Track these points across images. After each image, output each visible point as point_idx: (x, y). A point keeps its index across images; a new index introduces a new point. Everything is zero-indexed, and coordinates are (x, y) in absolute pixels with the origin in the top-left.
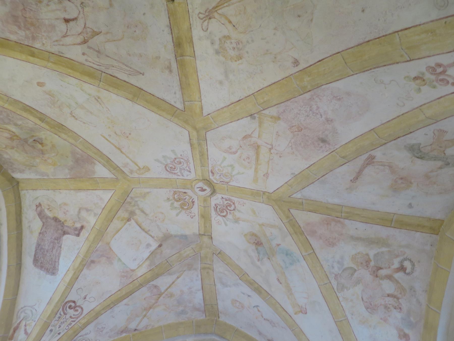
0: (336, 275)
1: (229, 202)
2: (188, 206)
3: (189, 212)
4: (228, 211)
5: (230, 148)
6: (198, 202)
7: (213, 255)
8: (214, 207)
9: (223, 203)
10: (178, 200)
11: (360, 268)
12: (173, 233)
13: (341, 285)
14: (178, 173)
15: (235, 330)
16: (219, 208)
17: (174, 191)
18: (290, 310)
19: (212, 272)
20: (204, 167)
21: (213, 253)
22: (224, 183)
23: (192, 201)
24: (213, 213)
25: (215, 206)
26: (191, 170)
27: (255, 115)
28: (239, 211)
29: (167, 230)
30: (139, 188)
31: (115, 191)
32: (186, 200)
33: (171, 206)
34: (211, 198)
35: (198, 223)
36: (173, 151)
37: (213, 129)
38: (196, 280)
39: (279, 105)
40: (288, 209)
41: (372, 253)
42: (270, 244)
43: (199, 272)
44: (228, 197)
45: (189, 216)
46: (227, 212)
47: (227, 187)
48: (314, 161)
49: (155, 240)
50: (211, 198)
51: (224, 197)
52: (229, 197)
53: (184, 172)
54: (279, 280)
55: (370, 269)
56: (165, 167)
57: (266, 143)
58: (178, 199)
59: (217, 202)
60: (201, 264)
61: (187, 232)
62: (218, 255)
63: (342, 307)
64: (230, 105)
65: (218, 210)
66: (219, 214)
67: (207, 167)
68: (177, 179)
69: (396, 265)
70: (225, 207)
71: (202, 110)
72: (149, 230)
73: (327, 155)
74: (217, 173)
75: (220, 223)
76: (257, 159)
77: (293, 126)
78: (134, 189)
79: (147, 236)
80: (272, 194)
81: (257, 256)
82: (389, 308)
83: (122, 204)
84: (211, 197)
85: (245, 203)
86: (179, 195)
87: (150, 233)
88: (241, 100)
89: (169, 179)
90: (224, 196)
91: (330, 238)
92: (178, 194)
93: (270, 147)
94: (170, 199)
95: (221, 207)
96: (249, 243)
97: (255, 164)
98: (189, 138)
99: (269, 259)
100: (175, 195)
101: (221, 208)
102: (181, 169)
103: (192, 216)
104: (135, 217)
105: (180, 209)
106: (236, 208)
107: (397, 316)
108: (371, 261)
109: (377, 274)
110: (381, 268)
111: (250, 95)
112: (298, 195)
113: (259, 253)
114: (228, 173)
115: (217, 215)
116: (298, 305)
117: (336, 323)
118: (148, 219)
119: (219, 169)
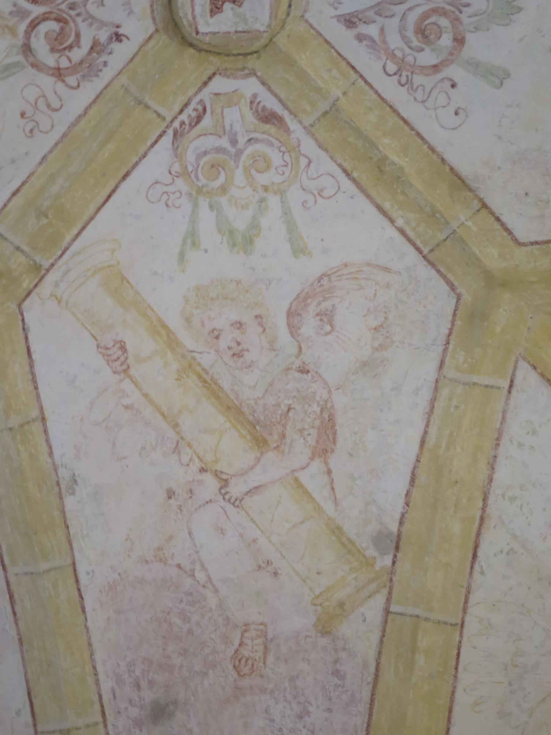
1: (77, 55)
9: (91, 17)
20: (326, 113)
22: (184, 117)
26: (350, 34)
27: (388, 560)
39: (370, 679)
44: (105, 70)
47: (159, 115)
51: (115, 46)
52: (107, 74)
57: (256, 488)
67: (312, 126)
70: (63, 7)
71: (542, 375)
73: (97, 682)
74: (257, 140)
77: (266, 650)
80: (14, 307)
85: (31, 131)
88: (472, 568)
97: (194, 359)
98: (494, 209)
106: (30, 69)
111: (465, 611)
119: (268, 167)
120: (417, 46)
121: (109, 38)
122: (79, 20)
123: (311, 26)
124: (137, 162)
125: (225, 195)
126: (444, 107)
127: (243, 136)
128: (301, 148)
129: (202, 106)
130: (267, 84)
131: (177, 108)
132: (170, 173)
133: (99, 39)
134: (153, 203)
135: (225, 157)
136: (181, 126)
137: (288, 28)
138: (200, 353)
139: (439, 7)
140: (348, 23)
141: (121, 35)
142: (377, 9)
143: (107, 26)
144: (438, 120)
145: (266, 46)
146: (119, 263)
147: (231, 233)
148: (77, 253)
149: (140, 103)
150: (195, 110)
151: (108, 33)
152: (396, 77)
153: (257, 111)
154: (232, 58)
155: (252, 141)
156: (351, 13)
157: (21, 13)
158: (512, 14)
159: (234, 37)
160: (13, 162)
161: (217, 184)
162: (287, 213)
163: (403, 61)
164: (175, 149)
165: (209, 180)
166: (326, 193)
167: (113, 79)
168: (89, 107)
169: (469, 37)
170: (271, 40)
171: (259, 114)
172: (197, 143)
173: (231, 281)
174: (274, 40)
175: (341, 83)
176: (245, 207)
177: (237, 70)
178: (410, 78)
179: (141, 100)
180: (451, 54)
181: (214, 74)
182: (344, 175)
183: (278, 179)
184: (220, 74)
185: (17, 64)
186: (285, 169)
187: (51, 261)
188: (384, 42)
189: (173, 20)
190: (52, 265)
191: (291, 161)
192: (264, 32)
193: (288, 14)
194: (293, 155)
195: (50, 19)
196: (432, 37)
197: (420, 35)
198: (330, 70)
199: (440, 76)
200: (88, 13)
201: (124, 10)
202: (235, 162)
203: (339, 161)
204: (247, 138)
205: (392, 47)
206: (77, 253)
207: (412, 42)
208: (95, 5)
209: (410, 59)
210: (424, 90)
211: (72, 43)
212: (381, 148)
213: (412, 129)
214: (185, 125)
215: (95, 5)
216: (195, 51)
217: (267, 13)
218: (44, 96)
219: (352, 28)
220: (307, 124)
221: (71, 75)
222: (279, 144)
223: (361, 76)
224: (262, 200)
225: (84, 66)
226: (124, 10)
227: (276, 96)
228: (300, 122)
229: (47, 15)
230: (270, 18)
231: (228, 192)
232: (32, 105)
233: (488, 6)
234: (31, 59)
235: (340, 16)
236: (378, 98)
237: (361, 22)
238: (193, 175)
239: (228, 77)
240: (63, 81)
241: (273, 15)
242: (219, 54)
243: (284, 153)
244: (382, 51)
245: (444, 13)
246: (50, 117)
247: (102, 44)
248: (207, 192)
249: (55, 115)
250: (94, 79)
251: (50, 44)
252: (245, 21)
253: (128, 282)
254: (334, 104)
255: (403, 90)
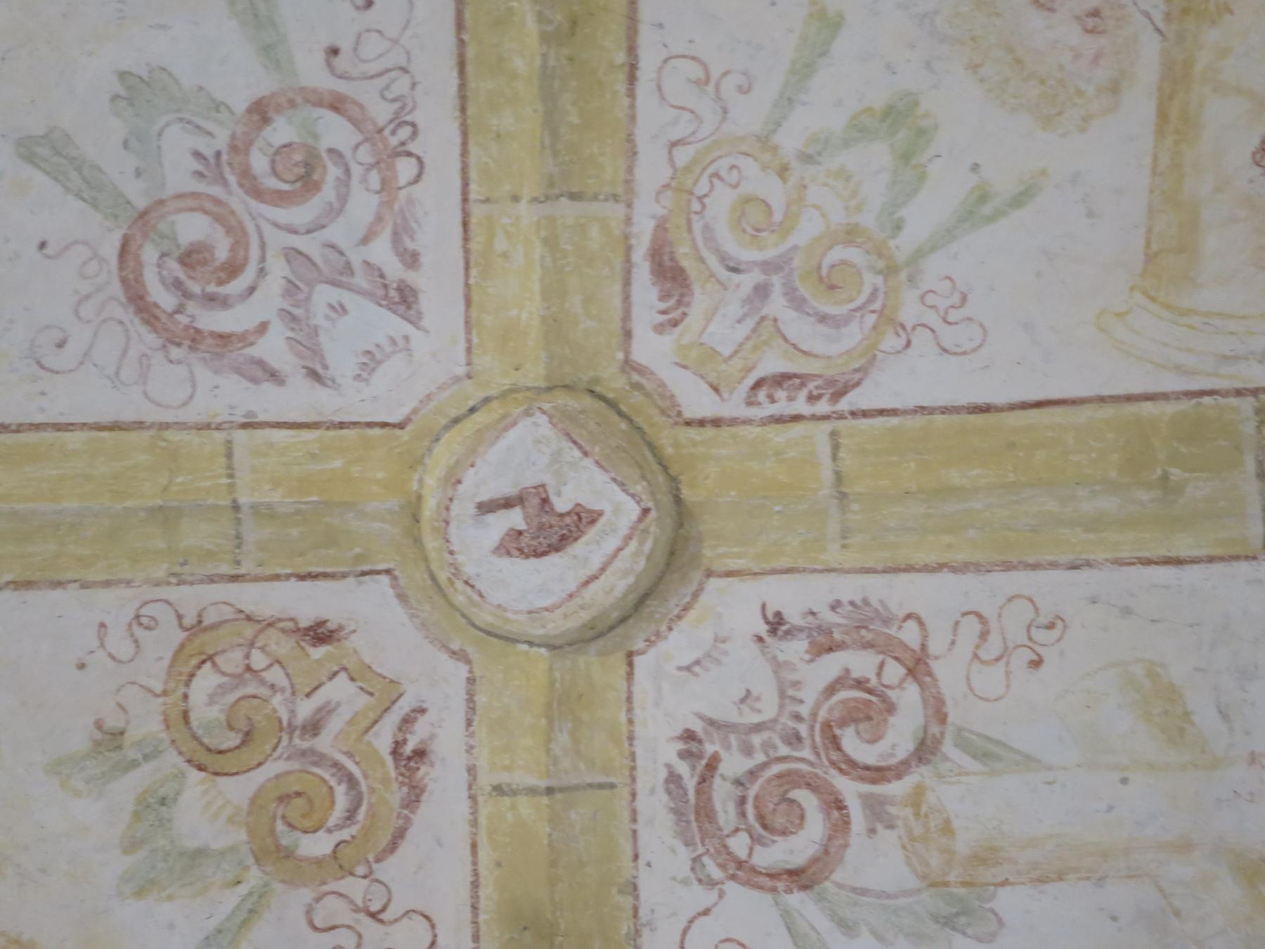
1: (861, 663)
2: (351, 815)
4: (849, 788)
9: (782, 694)
14: (263, 328)
16: (738, 783)
20: (574, 197)
22: (801, 406)
23: (395, 753)
25: (683, 768)
32: (324, 743)
33: (132, 845)
34: (630, 655)
44: (845, 599)
47: (836, 447)
50: (638, 660)
51: (794, 617)
52: (849, 588)
53: (342, 310)
65: (726, 814)
66: (740, 864)
67: (615, 198)
68: (241, 436)
70: (806, 753)
74: (723, 258)
84: (640, 645)
85: (1051, 626)
86: (238, 679)
92: (232, 661)
94: (133, 734)
95: (760, 758)
97: (1168, 17)
101: (764, 766)
105: (254, 876)
114: (851, 235)
115: (711, 883)
119: (747, 200)
120: (335, 164)
121: (789, 637)
122: (805, 710)
123: (469, 350)
124: (943, 413)
125: (857, 225)
126: (379, 31)
127: (738, 286)
128: (665, 181)
129: (756, 395)
130: (623, 328)
131: (797, 429)
132: (908, 344)
133: (807, 652)
134: (982, 326)
135: (798, 283)
136: (819, 397)
137: (507, 382)
138: (1148, 15)
139: (247, 192)
140: (411, 299)
141: (767, 622)
142: (344, 279)
143: (775, 658)
144: (408, 21)
145: (566, 387)
146: (1132, 289)
147: (906, 157)
148: (1179, 369)
149: (843, 496)
150: (772, 400)
151: (784, 645)
152: (411, 147)
153: (679, 303)
154: (639, 420)
155: (732, 264)
156: (390, 309)
157: (876, 810)
158: (141, 79)
159: (597, 449)
160: (1127, 611)
161: (852, 254)
162: (787, 101)
163: (378, 163)
164: (864, 371)
165: (859, 274)
166: (696, 72)
167: (848, 572)
168: (927, 569)
169: (240, 104)
170: (549, 389)
171: (682, 295)
172: (820, 347)
173: (982, 81)
174: (543, 384)
175: (506, 220)
176: (844, 175)
177: (648, 395)
178: (392, 126)
179: (837, 498)
180: (292, 104)
181: (688, 423)
182: (639, 74)
183: (750, 167)
184: (679, 414)
185: (963, 744)
186: (723, 173)
187: (1233, 401)
188: (379, 219)
189: (668, 565)
190: (1239, 393)
191: (701, 174)
192: (544, 412)
193: (487, 400)
194: (689, 183)
195: (845, 755)
196: (298, 157)
197: (316, 177)
198: (505, 255)
199: (342, 87)
200: (781, 706)
201: (726, 653)
202: (791, 259)
203: (626, 102)
204: (736, 278)
205: (376, 199)
206: (1179, 369)
207: (338, 179)
208: (758, 705)
209: (365, 155)
210: (387, 87)
211: (852, 687)
212: (538, 61)
213: (461, 43)
214: (810, 392)
215: (758, 705)
216: (681, 486)
217: (512, 435)
218: (976, 656)
219: (409, 286)
220: (620, 209)
221: (903, 645)
222: (695, 218)
223: (465, 200)
224: (807, 159)
225: (869, 636)
226: (726, 653)
227: (627, 298)
228: (628, 220)
229: (844, 766)
230: (514, 424)
231: (848, 224)
232: (1008, 664)
233: (167, 125)
234: (935, 729)
235: (411, 322)
236: (471, 142)
237: (386, 282)
238: (877, 305)
239: (672, 396)
240: (924, 647)
241: (505, 423)
242: (652, 447)
243: (700, 198)
244: (396, 206)
245: (246, 175)
246: (1000, 616)
247: (809, 640)
248: (880, 255)
249: (989, 612)
250: (874, 602)
251: (885, 720)
252: (556, 457)
253: (1148, 244)
254: (547, 198)
255: (418, 117)
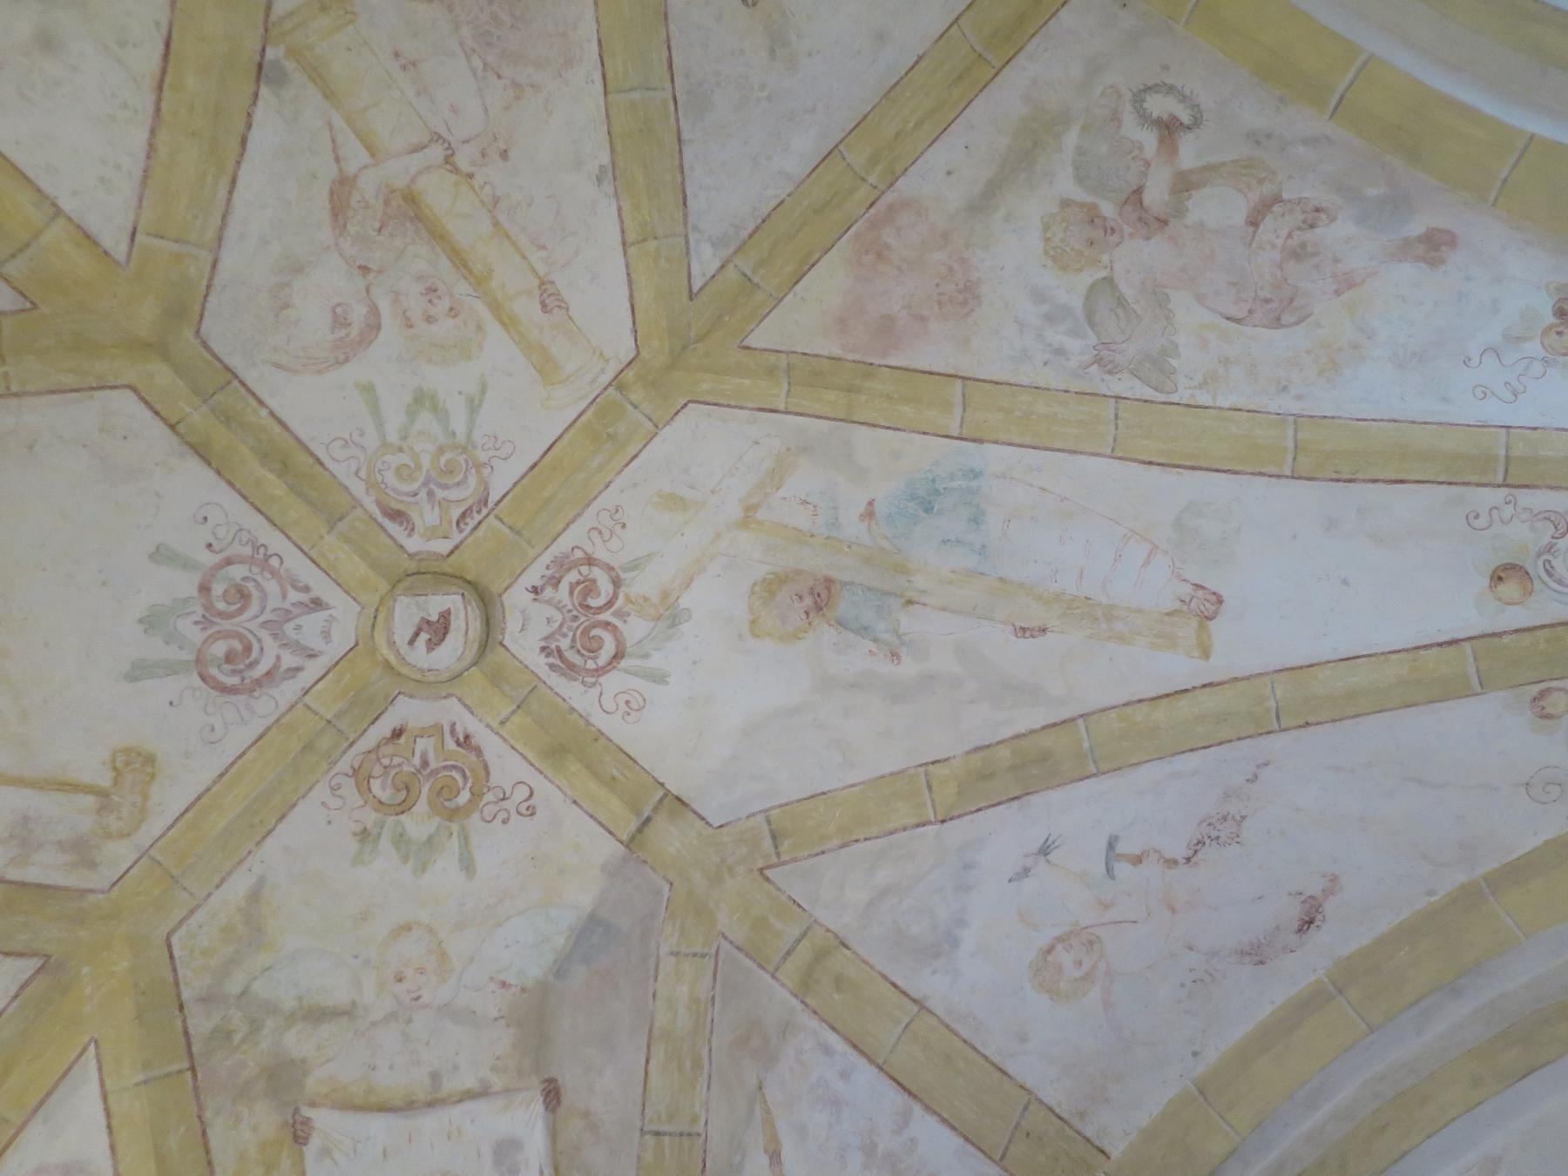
0: (1098, 360)
1: (573, 576)
2: (465, 777)
3: (496, 803)
4: (606, 616)
5: (339, 320)
6: (481, 720)
7: (768, 879)
8: (552, 667)
9: (559, 609)
10: (403, 794)
11: (1105, 258)
12: (535, 969)
13: (1147, 365)
14: (278, 658)
15: (1196, 1093)
16: (572, 647)
17: (350, 773)
18: (1178, 668)
19: (845, 951)
20: (340, 519)
21: (761, 870)
22: (478, 518)
23: (458, 744)
24: (573, 692)
25: (551, 660)
27: (271, 54)
28: (635, 565)
29: (504, 984)
30: (192, 912)
31: (96, 1041)
32: (434, 764)
34: (501, 644)
35: (574, 806)
36: (162, 555)
37: (209, 287)
38: (844, 1075)
40: (739, 347)
41: (1066, 185)
42: (849, 547)
43: (814, 1023)
44: (548, 562)
45: (514, 816)
46: (607, 625)
48: (586, 32)
49: (507, 1091)
50: (505, 643)
52: (547, 558)
54: (1024, 630)
55: (1128, 230)
56: (203, 679)
58: (399, 790)
59: (539, 630)
60: (777, 974)
61: (582, 896)
62: (778, 855)
63: (1240, 410)
64: (159, 101)
66: (597, 670)
67: (354, 507)
69: (1149, 140)
72: (435, 1077)
74: (407, 494)
75: (641, 701)
76: (460, 260)
78: (175, 940)
79: (456, 1113)
80: (644, 353)
81: (875, 650)
82: (1303, 246)
83: (189, 1074)
87: (450, 1085)
89: (274, 729)
90: (533, 576)
91: (937, 285)
92: (378, 770)
93: (436, 152)
94: (369, 826)
95: (571, 634)
96: (796, 636)
99: (910, 602)
100: (369, 789)
101: (574, 635)
102: (274, 628)
103: (526, 805)
104: (314, 1083)
105: (455, 827)
106: (615, 565)
107: (1340, 231)
108: (1094, 206)
109: (1156, 215)
110: (1139, 191)
112: (705, 261)
113: (865, 628)
115: (594, 684)
116: (1167, 614)
117: (1300, 478)
118: (374, 1024)
119: (398, 469)
